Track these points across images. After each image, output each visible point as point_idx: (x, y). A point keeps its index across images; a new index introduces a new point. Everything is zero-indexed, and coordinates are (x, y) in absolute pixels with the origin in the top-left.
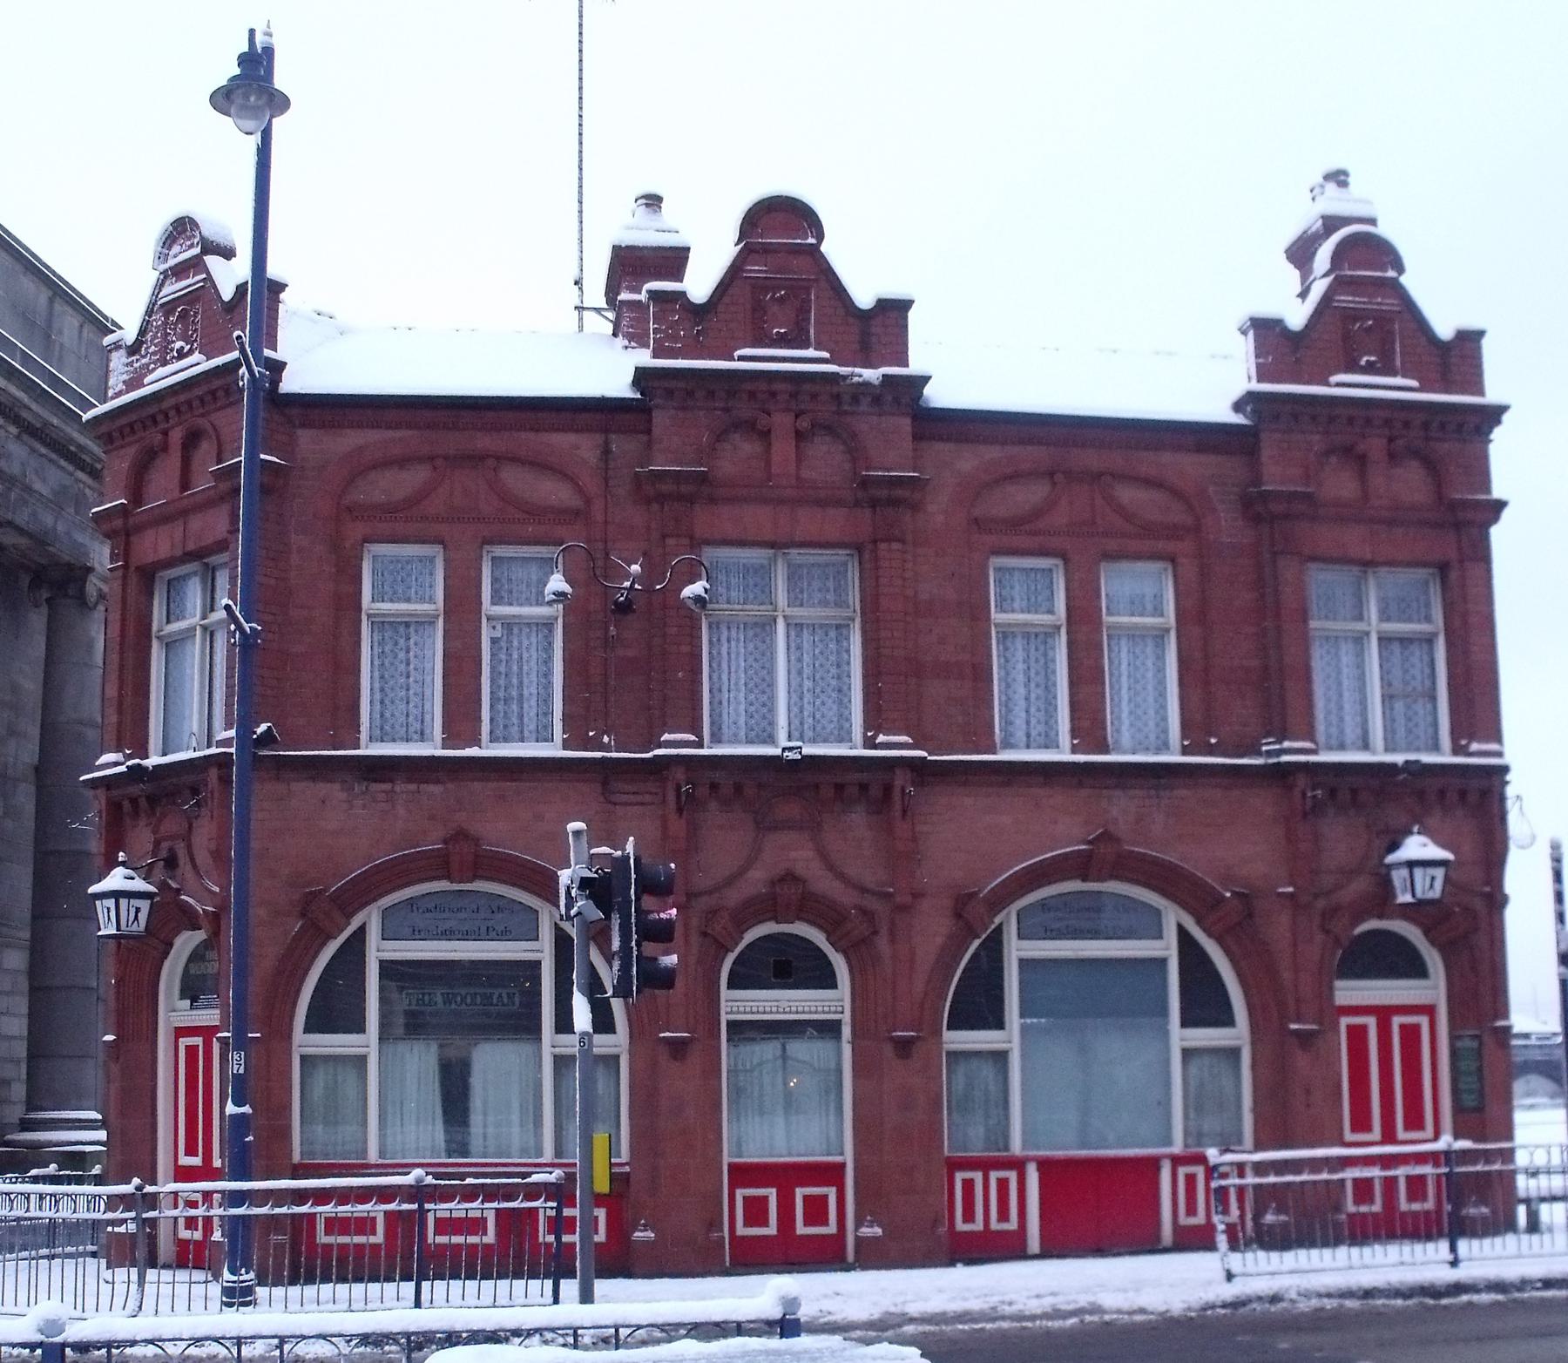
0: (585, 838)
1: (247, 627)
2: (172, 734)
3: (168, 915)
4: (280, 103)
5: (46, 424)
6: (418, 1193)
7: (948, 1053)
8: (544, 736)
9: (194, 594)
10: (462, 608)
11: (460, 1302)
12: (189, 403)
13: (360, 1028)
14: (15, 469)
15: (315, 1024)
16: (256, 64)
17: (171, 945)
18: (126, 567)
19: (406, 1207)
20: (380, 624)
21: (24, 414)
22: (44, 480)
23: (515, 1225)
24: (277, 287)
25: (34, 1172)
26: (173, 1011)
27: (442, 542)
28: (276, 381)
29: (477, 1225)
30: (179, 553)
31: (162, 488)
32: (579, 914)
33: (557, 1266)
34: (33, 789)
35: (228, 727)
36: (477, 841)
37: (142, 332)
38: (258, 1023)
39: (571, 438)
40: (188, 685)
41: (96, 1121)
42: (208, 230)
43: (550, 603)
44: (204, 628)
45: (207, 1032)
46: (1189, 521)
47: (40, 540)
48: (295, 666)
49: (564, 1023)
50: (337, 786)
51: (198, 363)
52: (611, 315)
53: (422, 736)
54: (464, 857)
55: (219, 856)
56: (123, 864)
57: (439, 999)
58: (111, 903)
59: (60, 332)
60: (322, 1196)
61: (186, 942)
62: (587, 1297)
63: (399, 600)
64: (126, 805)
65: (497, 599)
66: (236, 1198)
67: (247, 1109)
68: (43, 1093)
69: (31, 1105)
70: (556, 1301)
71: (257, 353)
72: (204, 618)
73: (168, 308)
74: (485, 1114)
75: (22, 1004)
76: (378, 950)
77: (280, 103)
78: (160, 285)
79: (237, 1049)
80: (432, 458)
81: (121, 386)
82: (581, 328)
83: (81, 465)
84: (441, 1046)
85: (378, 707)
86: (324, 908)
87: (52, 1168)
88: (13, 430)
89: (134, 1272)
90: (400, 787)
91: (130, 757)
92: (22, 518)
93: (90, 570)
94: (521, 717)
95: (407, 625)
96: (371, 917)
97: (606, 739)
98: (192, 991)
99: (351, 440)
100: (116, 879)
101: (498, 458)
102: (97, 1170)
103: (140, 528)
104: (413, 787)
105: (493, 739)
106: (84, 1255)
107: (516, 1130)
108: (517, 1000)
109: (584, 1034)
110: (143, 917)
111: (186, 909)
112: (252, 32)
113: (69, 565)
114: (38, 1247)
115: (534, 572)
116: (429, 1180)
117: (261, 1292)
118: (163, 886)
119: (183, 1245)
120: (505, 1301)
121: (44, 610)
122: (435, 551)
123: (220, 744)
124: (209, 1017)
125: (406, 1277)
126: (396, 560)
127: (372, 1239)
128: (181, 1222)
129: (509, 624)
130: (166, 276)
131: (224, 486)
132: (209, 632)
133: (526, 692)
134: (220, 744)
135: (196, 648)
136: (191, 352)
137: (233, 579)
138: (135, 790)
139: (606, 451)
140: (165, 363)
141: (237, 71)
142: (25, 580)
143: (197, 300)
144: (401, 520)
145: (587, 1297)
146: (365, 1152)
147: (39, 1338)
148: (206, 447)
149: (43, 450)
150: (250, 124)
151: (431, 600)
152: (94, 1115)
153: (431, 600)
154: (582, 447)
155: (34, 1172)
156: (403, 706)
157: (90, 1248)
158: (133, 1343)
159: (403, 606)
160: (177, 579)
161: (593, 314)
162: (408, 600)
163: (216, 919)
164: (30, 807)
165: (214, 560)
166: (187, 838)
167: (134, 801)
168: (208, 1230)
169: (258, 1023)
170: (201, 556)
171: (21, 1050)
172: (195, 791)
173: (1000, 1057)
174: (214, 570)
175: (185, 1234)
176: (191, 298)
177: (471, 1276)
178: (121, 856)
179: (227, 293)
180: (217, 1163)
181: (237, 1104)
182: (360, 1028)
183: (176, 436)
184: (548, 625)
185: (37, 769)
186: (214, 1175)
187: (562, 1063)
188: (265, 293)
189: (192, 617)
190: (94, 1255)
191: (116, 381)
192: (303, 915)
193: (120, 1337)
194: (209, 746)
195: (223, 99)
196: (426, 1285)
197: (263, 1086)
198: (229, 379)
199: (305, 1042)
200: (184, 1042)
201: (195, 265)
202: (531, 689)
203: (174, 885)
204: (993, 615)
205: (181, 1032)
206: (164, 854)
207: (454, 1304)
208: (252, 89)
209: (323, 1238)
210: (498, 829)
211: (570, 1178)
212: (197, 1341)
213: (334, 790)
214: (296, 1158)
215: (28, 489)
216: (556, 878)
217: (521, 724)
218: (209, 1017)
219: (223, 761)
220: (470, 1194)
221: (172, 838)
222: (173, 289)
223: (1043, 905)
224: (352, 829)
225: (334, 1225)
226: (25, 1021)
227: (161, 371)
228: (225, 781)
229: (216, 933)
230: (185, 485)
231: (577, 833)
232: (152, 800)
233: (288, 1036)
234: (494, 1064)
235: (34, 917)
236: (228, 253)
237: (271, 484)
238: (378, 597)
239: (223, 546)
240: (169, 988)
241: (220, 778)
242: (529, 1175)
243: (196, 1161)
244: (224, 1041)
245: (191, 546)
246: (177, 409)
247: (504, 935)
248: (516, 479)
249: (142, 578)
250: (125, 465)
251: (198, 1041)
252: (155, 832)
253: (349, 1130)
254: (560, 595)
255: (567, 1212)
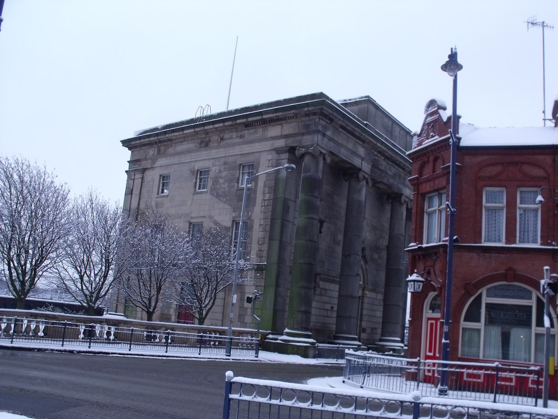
0: (549, 272)
1: (452, 210)
2: (429, 238)
3: (427, 287)
4: (460, 67)
5: (391, 156)
6: (497, 369)
7: (463, 329)
8: (535, 241)
9: (436, 201)
10: (511, 205)
11: (483, 400)
12: (435, 149)
13: (479, 321)
14: (383, 168)
15: (466, 320)
16: (453, 56)
17: (427, 295)
18: (418, 193)
19: (493, 373)
20: (488, 209)
21: (386, 154)
22: (391, 171)
23: (522, 382)
24: (459, 117)
25: (387, 353)
26: (427, 313)
27: (505, 186)
28: (459, 143)
29: (510, 380)
30: (432, 190)
31: (427, 172)
32: (547, 293)
33: (536, 395)
34: (386, 252)
35: (446, 236)
36: (515, 271)
37: (422, 131)
38: (452, 318)
39: (543, 157)
40: (434, 226)
41: (356, 338)
42: (439, 103)
43: (537, 204)
44: (439, 210)
45: (437, 319)
46: (546, 175)
47: (389, 186)
48: (465, 221)
49: (540, 323)
50: (475, 254)
51: (437, 139)
52: (554, 121)
53: (499, 241)
54: (511, 275)
55: (443, 272)
56: (416, 273)
57: (502, 315)
58: (412, 283)
59: (395, 132)
60: (469, 367)
61: (432, 295)
62: (545, 405)
63: (493, 203)
64: (417, 257)
65: (521, 203)
66: (445, 366)
67: (448, 341)
68: (386, 332)
69: (382, 335)
70: (536, 405)
71: (455, 135)
72: (439, 207)
73: (429, 124)
74: (514, 348)
75: (381, 309)
76: (485, 300)
77: (460, 67)
78: (426, 118)
79: (446, 324)
80: (503, 164)
81: (416, 145)
82: (545, 125)
83: (400, 167)
84: (502, 328)
85: (487, 232)
86: (471, 287)
87: (391, 352)
88: (383, 158)
89: (416, 383)
90: (493, 255)
91: (418, 244)
92: (385, 181)
93: (402, 194)
94: (528, 236)
95: (495, 210)
96: (484, 291)
97: (554, 243)
98: (433, 308)
99: (480, 159)
100: (414, 277)
101: (522, 163)
102: (403, 354)
103: (421, 183)
104: (497, 255)
105: (520, 242)
106: (397, 376)
107: (523, 353)
108: (525, 316)
109: (548, 328)
110: (421, 287)
111: (432, 285)
112: (452, 49)
113: (397, 193)
114: (386, 373)
115: (532, 195)
116: (500, 366)
117: (450, 392)
118: (426, 279)
119: (425, 376)
120: (525, 403)
121: (390, 205)
122: (504, 189)
123: (443, 241)
124: (438, 315)
125: (492, 392)
126: (492, 192)
127: (479, 380)
128: (426, 371)
129: (525, 210)
130: (428, 116)
131: (446, 171)
132: (440, 211)
133: (530, 229)
134: (443, 241)
135: (436, 217)
136: (435, 136)
137: (448, 197)
138: (420, 253)
139: (554, 160)
140: (428, 139)
141: (448, 59)
142: (385, 197)
143: (437, 122)
144: (494, 181)
145: (545, 405)
146: (479, 356)
147: (413, 400)
148: (440, 161)
149: (390, 163)
150: (452, 74)
151: (502, 203)
152: (399, 339)
153: (502, 203)
154: (548, 159)
155: (387, 353)
156: (494, 232)
157: (399, 375)
158: (439, 405)
159: (494, 205)
160: (432, 197)
161: (549, 121)
162: (496, 203)
163: (441, 289)
164: (385, 257)
165: (441, 192)
166: (433, 266)
167: (419, 256)
168: (434, 374)
169: (452, 318)
170: (438, 191)
171: (381, 320)
172: (436, 254)
173: (479, 331)
174: (442, 194)
175: (427, 374)
176: (435, 121)
177: (511, 394)
178: (416, 271)
179: (445, 119)
180: (437, 355)
181: (446, 339)
182: (479, 321)
183: (431, 158)
184: (536, 210)
185: (387, 247)
186: (434, 357)
187: (538, 335)
188: (455, 118)
189: (435, 207)
190: (400, 376)
191: (414, 144)
192: (465, 289)
193: (435, 403)
194: (440, 242)
195: (445, 67)
196: (497, 396)
197: (452, 335)
198: (446, 143)
199: (464, 324)
200: (430, 322)
201: (436, 112)
202: (531, 228)
203: (429, 279)
204: (519, 205)
205: (429, 319)
206: (427, 271)
207: (507, 403)
208: (452, 65)
209: (530, 385)
210: (521, 268)
211: (542, 369)
212: (456, 407)
213: (474, 255)
214: (460, 356)
215: (386, 173)
216: (539, 283)
217: (528, 238)
218: (438, 315)
219: (444, 246)
220: (511, 371)
221: (429, 266)
222: (430, 119)
223: (495, 287)
224: (479, 266)
225: (469, 375)
226: (382, 313)
227: (427, 141)
228: (445, 252)
229: (441, 293)
230: (434, 171)
231: (547, 270)
232: (424, 256)
233: (458, 322)
234: (518, 335)
235: (386, 286)
236: (445, 109)
237: (458, 171)
238: (487, 202)
239: (444, 188)
240: (427, 306)
241: (443, 251)
242: (529, 367)
243: (431, 354)
244: (442, 323)
245: (435, 188)
246: (432, 151)
247: (522, 298)
248: (527, 169)
249: (421, 197)
250: (417, 166)
251: (434, 322)
252: (425, 264)
253: (474, 350)
254: (541, 202)
255: (541, 379)
